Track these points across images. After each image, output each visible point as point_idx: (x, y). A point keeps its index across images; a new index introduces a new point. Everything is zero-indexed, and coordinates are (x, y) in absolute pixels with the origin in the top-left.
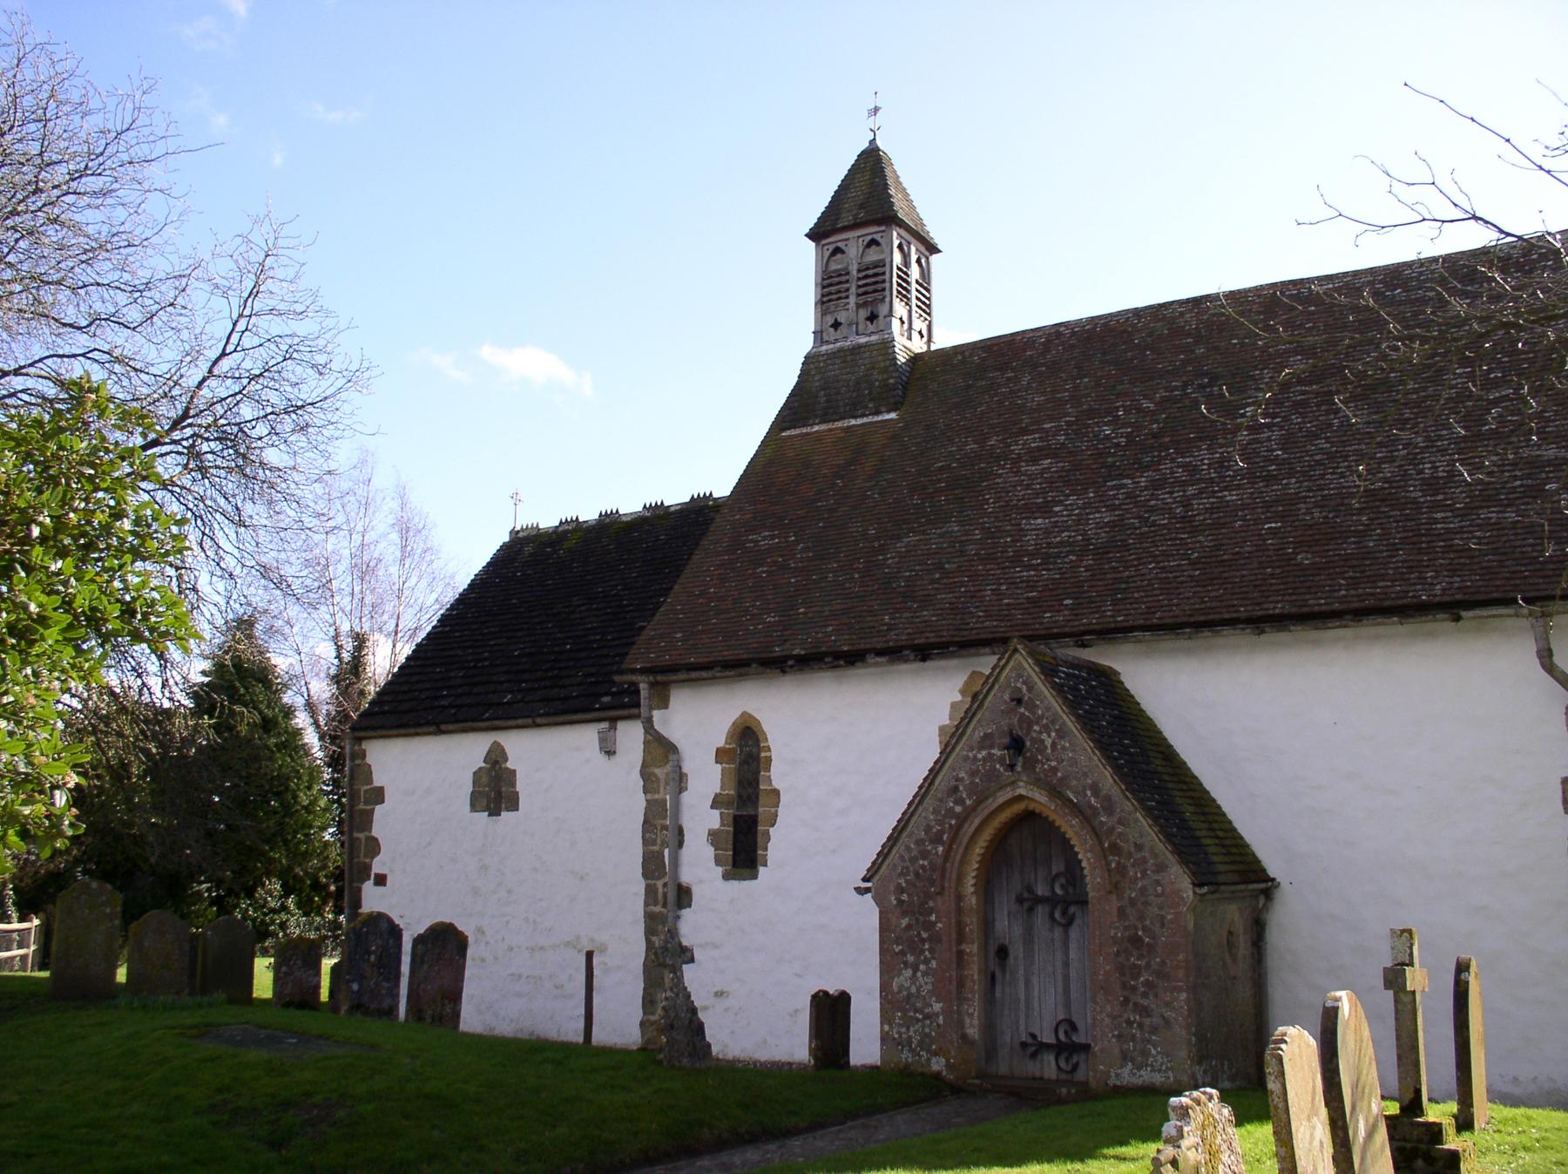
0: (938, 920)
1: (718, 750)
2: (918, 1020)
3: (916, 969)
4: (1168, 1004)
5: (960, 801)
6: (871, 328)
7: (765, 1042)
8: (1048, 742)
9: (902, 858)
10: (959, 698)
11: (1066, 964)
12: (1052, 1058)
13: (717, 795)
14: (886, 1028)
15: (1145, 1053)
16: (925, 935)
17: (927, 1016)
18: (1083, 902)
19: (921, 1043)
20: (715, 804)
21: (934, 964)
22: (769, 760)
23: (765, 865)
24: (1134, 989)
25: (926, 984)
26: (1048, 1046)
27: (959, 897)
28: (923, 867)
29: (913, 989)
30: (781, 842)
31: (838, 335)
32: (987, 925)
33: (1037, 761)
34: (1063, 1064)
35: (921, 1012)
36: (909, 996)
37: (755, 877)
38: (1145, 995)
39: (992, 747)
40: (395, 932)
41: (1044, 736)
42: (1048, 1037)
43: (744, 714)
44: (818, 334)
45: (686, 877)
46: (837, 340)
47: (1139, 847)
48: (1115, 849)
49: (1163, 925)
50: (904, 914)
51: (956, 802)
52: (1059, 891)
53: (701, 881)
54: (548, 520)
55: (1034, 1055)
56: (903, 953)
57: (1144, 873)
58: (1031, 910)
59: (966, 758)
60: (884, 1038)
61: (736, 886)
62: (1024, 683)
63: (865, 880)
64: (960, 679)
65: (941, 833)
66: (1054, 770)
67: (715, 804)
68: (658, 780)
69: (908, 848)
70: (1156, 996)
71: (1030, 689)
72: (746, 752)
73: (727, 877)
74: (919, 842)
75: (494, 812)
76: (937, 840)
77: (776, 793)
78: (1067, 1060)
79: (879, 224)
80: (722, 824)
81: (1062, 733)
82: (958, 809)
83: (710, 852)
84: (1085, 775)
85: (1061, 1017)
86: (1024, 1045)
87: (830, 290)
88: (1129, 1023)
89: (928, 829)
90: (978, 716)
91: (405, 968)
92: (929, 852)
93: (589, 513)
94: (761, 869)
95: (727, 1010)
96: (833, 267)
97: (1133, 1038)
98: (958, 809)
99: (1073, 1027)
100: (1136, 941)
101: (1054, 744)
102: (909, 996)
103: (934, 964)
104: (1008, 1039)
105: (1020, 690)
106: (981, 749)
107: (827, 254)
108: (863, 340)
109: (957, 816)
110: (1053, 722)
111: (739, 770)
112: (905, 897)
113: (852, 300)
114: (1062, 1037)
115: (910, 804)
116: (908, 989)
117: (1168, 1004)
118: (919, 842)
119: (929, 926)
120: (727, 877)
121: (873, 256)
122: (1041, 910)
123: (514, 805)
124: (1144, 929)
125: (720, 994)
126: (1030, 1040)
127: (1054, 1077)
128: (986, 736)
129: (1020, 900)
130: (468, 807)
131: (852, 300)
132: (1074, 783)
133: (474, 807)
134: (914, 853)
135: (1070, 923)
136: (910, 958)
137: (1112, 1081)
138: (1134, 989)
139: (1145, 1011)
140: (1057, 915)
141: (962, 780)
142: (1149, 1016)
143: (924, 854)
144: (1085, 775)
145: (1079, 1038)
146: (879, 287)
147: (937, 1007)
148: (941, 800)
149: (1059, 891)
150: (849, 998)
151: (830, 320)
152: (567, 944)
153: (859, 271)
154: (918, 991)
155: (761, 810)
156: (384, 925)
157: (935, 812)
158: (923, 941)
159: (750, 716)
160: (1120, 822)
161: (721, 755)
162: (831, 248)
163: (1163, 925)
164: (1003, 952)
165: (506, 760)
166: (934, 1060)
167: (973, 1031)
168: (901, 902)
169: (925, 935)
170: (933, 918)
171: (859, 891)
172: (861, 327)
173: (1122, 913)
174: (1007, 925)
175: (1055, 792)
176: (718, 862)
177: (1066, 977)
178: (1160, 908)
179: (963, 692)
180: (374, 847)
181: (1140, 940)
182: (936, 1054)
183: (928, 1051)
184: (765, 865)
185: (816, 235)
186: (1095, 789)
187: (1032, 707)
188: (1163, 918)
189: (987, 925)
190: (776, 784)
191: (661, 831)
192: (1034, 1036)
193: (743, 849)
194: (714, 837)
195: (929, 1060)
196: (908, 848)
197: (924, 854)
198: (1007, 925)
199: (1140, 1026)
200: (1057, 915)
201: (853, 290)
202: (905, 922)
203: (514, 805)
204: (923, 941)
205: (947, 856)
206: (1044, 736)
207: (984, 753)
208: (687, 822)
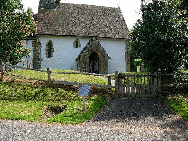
20: (46, 50)
30: (54, 54)
45: (42, 58)
53: (44, 58)
61: (49, 59)
64: (76, 39)
67: (46, 50)
76: (87, 54)
77: (54, 49)
120: (47, 58)
139: (105, 69)
147: (86, 69)
176: (46, 56)
193: (49, 54)
194: (45, 53)
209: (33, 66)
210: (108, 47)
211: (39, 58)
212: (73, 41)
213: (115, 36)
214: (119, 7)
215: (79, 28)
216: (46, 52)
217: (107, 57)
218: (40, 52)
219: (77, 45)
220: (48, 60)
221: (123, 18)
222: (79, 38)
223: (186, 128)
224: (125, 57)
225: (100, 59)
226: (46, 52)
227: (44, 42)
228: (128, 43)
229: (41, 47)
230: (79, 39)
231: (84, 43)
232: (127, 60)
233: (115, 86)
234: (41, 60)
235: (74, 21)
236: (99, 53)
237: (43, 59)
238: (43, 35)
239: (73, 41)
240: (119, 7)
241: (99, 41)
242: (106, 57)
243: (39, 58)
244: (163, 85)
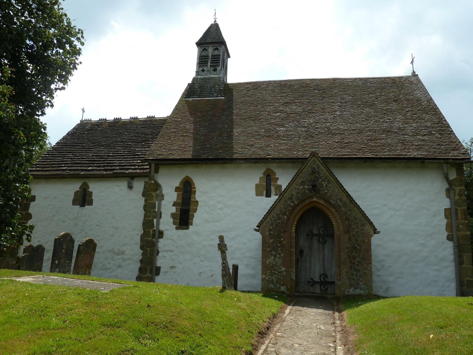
0: (284, 240)
1: (176, 188)
2: (276, 274)
3: (275, 256)
4: (365, 269)
5: (293, 202)
6: (215, 73)
7: (188, 283)
8: (324, 184)
9: (271, 220)
10: (262, 176)
11: (324, 256)
12: (318, 286)
13: (175, 202)
14: (264, 276)
15: (358, 284)
16: (279, 245)
17: (280, 272)
18: (332, 236)
19: (277, 282)
20: (174, 204)
21: (282, 255)
22: (195, 192)
23: (192, 225)
24: (354, 263)
25: (279, 261)
26: (317, 282)
27: (291, 233)
28: (279, 223)
29: (274, 263)
30: (198, 218)
31: (204, 73)
32: (297, 243)
33: (321, 190)
34: (322, 288)
35: (277, 271)
36: (273, 265)
37: (188, 229)
38: (357, 265)
39: (304, 185)
40: (72, 241)
41: (323, 183)
42: (317, 279)
43: (187, 177)
44: (197, 73)
45: (162, 228)
46: (203, 75)
47: (356, 218)
48: (347, 219)
49: (364, 243)
50: (271, 238)
51: (291, 202)
52: (321, 232)
53: (167, 230)
54: (95, 118)
55: (312, 286)
56: (270, 251)
57: (357, 227)
58: (312, 238)
59: (295, 188)
60: (263, 280)
61: (181, 232)
62: (316, 166)
63: (257, 226)
64: (263, 170)
65: (285, 212)
66: (326, 193)
67: (174, 204)
68: (153, 196)
69: (273, 217)
70: (362, 265)
71: (318, 168)
72: (187, 190)
73: (177, 228)
74: (277, 215)
75: (83, 205)
76: (284, 214)
77: (197, 202)
78: (324, 287)
79: (219, 44)
80: (176, 211)
81: (329, 182)
82: (292, 204)
83: (171, 220)
84: (337, 195)
85: (322, 272)
86: (309, 282)
87: (202, 61)
88: (352, 274)
89: (281, 210)
90: (300, 175)
91: (75, 254)
92: (281, 218)
93: (110, 117)
94: (190, 226)
95: (175, 272)
96: (203, 54)
97: (354, 279)
98: (292, 204)
99: (326, 276)
100: (355, 248)
101: (326, 185)
102: (273, 265)
103: (282, 255)
104: (303, 280)
105: (315, 168)
106: (300, 186)
107: (201, 50)
108: (212, 76)
109: (292, 207)
110: (326, 178)
111: (183, 194)
112: (272, 232)
113: (209, 64)
114: (322, 279)
115: (275, 202)
116: (272, 263)
117: (365, 269)
118: (277, 215)
119: (281, 242)
120: (177, 228)
121: (216, 52)
122: (315, 240)
123: (91, 203)
124: (357, 244)
125: (172, 267)
126: (311, 281)
127: (319, 292)
128: (303, 182)
129: (308, 235)
130: (72, 204)
131: (209, 64)
132: (333, 197)
133: (74, 204)
134: (276, 218)
135: (325, 243)
136: (273, 253)
137: (346, 293)
138: (354, 263)
139: (358, 271)
140: (321, 240)
141: (293, 195)
142: (359, 272)
143: (279, 219)
144: (337, 195)
145: (329, 280)
146: (218, 62)
147: (283, 269)
148: (286, 201)
149: (321, 232)
150: (137, 278)
151: (201, 69)
152: (109, 251)
153: (212, 56)
154: (276, 264)
155: (191, 207)
156: (69, 238)
157: (284, 205)
158: (279, 247)
159: (189, 177)
160: (349, 210)
161: (177, 189)
162: (203, 48)
163: (364, 243)
164: (301, 252)
165: (89, 188)
166: (282, 287)
167: (294, 277)
168: (270, 234)
169: (279, 245)
170: (282, 239)
171: (256, 230)
172: (211, 72)
173: (350, 239)
174: (303, 243)
175: (326, 201)
176: (174, 223)
177: (323, 261)
178: (363, 238)
179: (264, 174)
180: (29, 217)
181: (356, 247)
182: (283, 285)
183: (280, 284)
184: (192, 225)
185: (199, 44)
186: (341, 200)
187: (319, 173)
188: (364, 241)
189: (297, 243)
190: (197, 199)
191: (151, 213)
192: (312, 279)
193: (184, 219)
194: (173, 215)
195: (280, 287)
196: (273, 217)
197: (279, 219)
198: (303, 243)
199: (356, 275)
200: (321, 240)
201: (210, 61)
202: (271, 241)
203: (91, 203)
204: (279, 247)
205: (288, 219)
206: (323, 183)
207: (302, 187)
208: (163, 210)
209: (142, 252)
210: (372, 194)
211: (155, 228)
212: (254, 178)
213: (398, 152)
214: (414, 72)
215: (278, 137)
216: (174, 210)
217: (363, 225)
218: (156, 210)
219: (266, 188)
220: (179, 236)
221: (430, 100)
222: (273, 167)
223: (47, 11)
224: (449, 227)
225: (336, 233)
226: (174, 210)
227: (169, 184)
228: (453, 175)
229: (162, 197)
230: (275, 170)
231: (284, 180)
232: (455, 238)
233: (449, 207)
234: (157, 234)
235: (267, 120)
236: (333, 210)
237: (165, 233)
238: (168, 162)
239: (254, 178)
240: (414, 72)
241: (342, 180)
242: (360, 227)
243: (155, 228)
244: (351, 282)
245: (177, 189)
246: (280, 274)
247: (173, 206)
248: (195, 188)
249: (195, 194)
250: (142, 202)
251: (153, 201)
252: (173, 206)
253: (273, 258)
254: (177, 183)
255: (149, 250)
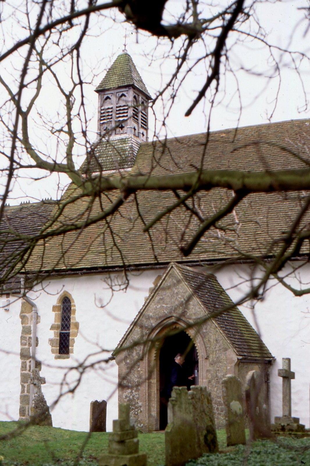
20: (52, 328)
22: (75, 310)
67: (52, 328)
72: (66, 306)
83: (50, 348)
120: (57, 358)
159: (67, 292)
161: (54, 308)
176: (53, 351)
211: (32, 336)
245: (54, 308)
246: (136, 410)
247: (51, 329)
248: (75, 306)
249: (74, 313)
250: (19, 328)
251: (29, 325)
252: (51, 329)
253: (129, 391)
254: (55, 300)
255: (26, 386)
